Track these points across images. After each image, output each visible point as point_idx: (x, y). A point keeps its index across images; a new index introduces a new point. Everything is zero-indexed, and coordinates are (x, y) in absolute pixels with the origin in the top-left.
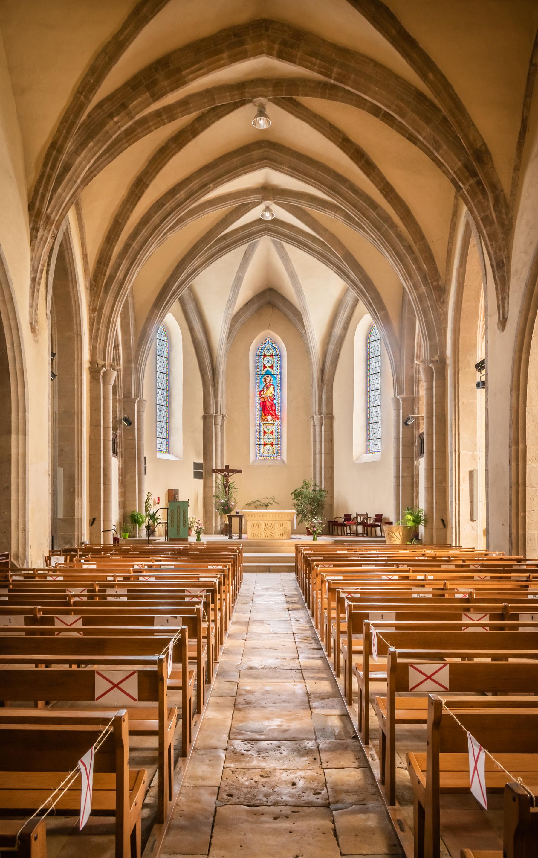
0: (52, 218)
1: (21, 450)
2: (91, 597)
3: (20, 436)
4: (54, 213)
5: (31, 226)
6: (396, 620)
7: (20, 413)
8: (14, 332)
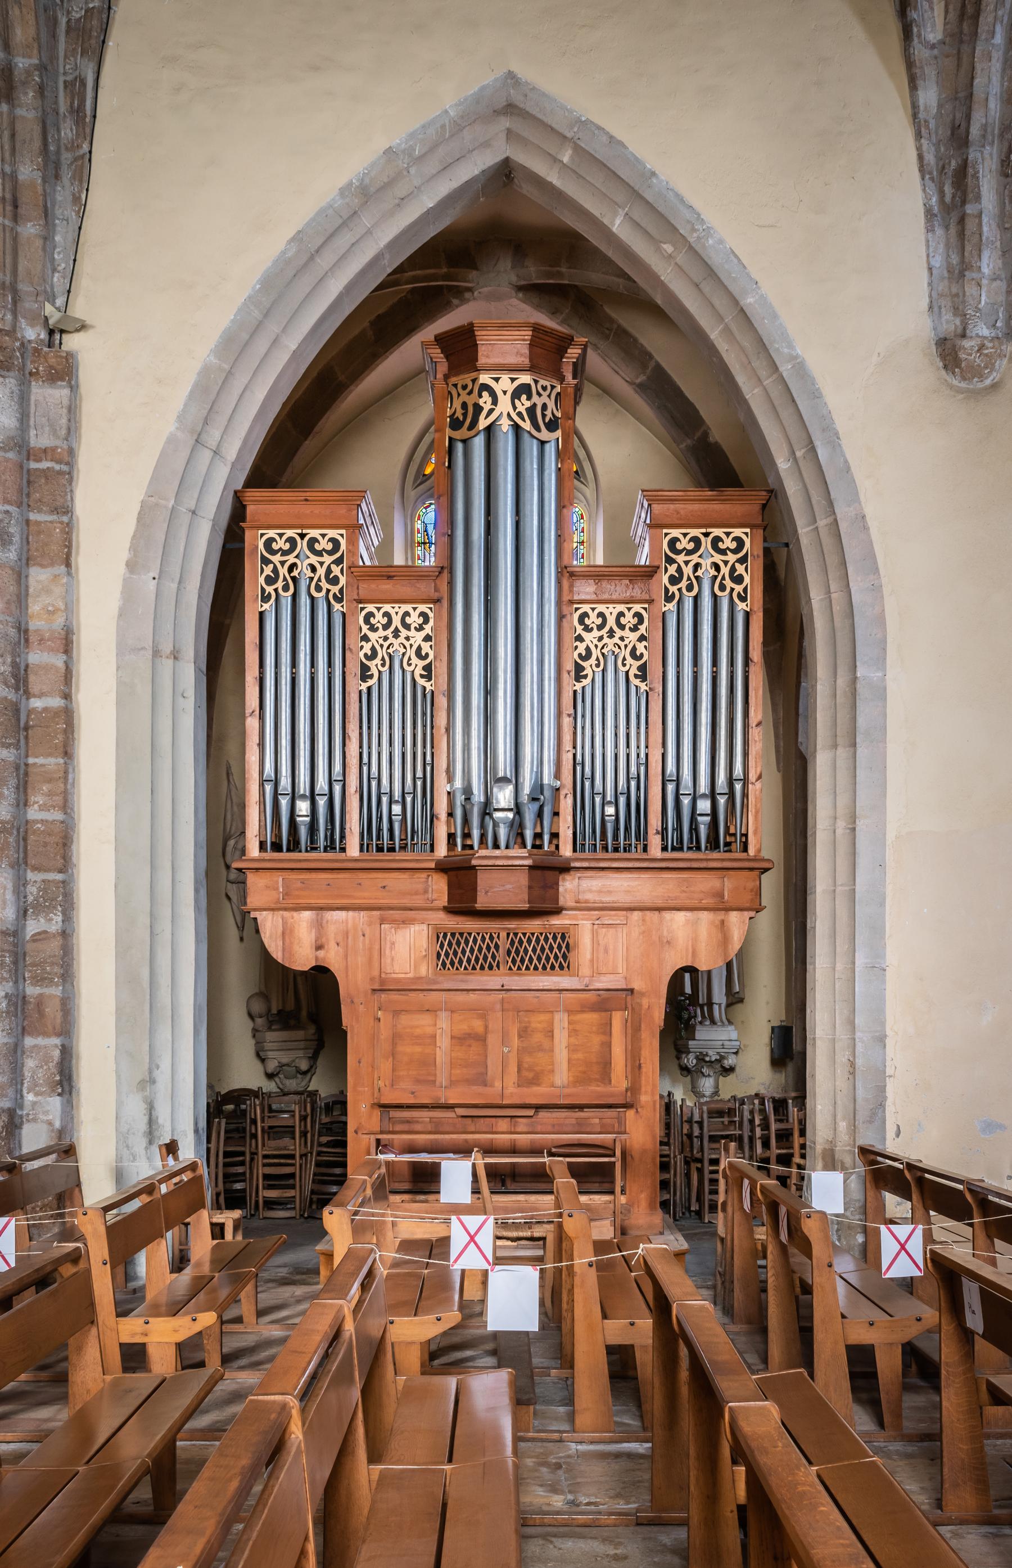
3: (842, 753)
8: (786, 414)
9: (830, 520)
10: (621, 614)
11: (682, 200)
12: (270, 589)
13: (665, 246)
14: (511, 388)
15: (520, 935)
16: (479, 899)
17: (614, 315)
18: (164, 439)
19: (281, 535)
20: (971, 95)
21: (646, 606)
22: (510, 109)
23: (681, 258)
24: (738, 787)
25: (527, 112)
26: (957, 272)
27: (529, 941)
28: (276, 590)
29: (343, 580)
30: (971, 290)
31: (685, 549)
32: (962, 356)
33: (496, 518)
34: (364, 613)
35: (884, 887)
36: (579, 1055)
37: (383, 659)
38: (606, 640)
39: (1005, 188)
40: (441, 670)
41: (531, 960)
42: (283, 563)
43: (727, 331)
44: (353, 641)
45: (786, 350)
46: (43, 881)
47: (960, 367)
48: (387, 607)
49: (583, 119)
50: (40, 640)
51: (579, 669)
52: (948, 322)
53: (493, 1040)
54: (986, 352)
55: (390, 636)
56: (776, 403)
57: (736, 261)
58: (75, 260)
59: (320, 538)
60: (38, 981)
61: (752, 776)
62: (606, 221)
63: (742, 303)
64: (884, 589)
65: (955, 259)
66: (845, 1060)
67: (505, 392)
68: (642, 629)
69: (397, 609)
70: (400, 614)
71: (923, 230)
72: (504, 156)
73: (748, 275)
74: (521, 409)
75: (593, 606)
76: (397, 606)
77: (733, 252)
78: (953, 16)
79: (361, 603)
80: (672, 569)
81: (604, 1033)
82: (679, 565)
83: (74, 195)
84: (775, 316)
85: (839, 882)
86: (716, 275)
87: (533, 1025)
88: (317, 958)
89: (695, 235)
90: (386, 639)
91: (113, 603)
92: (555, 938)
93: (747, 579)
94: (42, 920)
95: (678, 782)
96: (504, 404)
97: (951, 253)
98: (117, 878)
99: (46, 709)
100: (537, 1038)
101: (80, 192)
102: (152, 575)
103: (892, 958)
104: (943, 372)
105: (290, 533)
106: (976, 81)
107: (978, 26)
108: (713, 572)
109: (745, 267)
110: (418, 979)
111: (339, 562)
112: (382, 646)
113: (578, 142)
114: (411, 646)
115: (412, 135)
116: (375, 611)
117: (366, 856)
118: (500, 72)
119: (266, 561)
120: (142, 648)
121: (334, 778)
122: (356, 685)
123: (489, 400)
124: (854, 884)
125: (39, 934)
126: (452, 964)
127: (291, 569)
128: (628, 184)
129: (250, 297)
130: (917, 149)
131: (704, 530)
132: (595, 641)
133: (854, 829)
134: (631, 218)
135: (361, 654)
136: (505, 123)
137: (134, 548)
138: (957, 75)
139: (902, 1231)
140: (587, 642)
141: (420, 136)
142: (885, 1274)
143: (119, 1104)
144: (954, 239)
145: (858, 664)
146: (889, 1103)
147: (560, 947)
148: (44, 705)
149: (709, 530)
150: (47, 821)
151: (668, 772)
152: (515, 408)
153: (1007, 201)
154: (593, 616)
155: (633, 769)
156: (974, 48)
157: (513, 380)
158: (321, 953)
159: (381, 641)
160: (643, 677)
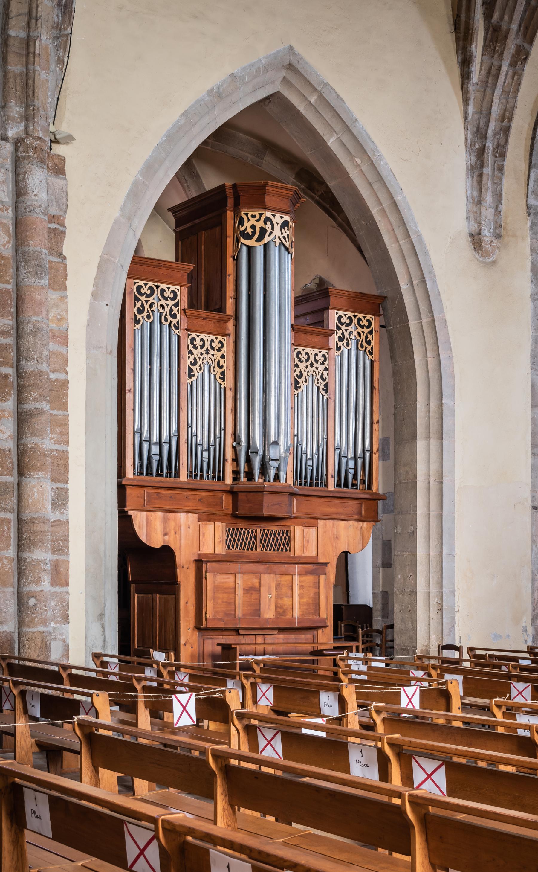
0: (504, 27)
1: (434, 467)
2: (160, 684)
3: (434, 442)
4: (506, 18)
5: (460, 58)
6: (70, 686)
7: (432, 400)
8: (410, 261)
9: (430, 319)
10: (212, 341)
11: (369, 137)
12: (139, 316)
13: (357, 160)
14: (281, 222)
15: (266, 531)
16: (127, 504)
17: (196, 165)
18: (113, 220)
19: (146, 285)
20: (490, 114)
21: (328, 351)
22: (290, 67)
23: (364, 168)
24: (368, 454)
25: (299, 71)
26: (476, 200)
27: (271, 535)
28: (143, 317)
29: (179, 316)
30: (483, 211)
31: (345, 322)
32: (483, 245)
33: (269, 293)
34: (190, 337)
35: (454, 513)
36: (305, 600)
37: (200, 366)
38: (309, 368)
39: (495, 163)
40: (230, 375)
41: (272, 546)
42: (147, 302)
43: (383, 210)
44: (184, 352)
45: (414, 228)
46: (57, 488)
47: (482, 250)
48: (202, 336)
49: (325, 82)
50: (53, 336)
51: (190, 370)
52: (472, 225)
53: (264, 590)
54: (493, 244)
55: (204, 353)
56: (405, 254)
57: (392, 176)
58: (58, 98)
59: (166, 290)
60: (55, 551)
61: (375, 450)
62: (325, 138)
63: (395, 199)
64: (454, 359)
65: (476, 194)
66: (435, 603)
67: (278, 224)
68: (223, 350)
69: (207, 337)
70: (209, 341)
71: (465, 177)
72: (278, 90)
73: (398, 184)
74: (285, 235)
75: (320, 350)
76: (208, 335)
77: (392, 171)
78: (483, 72)
79: (189, 331)
80: (340, 333)
81: (315, 588)
82: (142, 303)
83: (59, 57)
84: (409, 209)
85: (431, 510)
86: (383, 181)
87: (282, 583)
88: (164, 541)
89: (375, 158)
90: (202, 354)
91: (84, 317)
92: (283, 534)
93: (372, 344)
94: (58, 513)
95: (197, 436)
96: (277, 230)
97: (474, 190)
98: (86, 488)
99: (57, 380)
100: (284, 589)
101: (63, 57)
102: (106, 303)
103: (457, 550)
104: (473, 251)
105: (150, 284)
106: (493, 108)
107: (497, 81)
108: (358, 337)
109: (396, 180)
110: (215, 555)
111: (177, 305)
112: (200, 358)
113: (323, 94)
114: (319, 372)
115: (244, 69)
116: (196, 337)
117: (339, 489)
118: (286, 45)
119: (137, 299)
120: (101, 347)
121: (366, 449)
122: (185, 380)
123: (270, 227)
124: (442, 511)
125: (55, 521)
126: (233, 546)
127: (151, 306)
128: (345, 123)
129: (160, 144)
130: (465, 135)
131: (354, 314)
132: (304, 368)
133: (442, 482)
134: (341, 141)
135: (189, 362)
136: (284, 73)
137: (96, 284)
138: (482, 102)
139: (184, 698)
140: (300, 368)
141: (248, 71)
142: (176, 725)
143: (87, 629)
144: (475, 184)
145: (443, 396)
146: (456, 625)
147: (285, 539)
148: (56, 378)
149: (356, 314)
150: (59, 450)
151: (193, 432)
152: (282, 234)
153: (496, 169)
154: (198, 340)
155: (321, 441)
156: (494, 92)
157: (282, 217)
158: (167, 538)
159: (199, 355)
160: (326, 391)
